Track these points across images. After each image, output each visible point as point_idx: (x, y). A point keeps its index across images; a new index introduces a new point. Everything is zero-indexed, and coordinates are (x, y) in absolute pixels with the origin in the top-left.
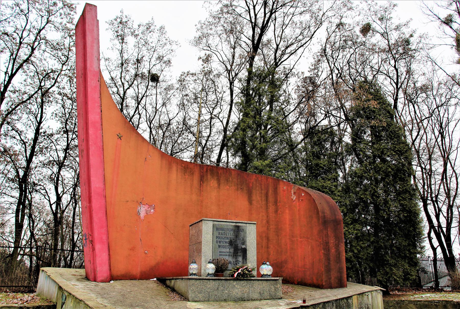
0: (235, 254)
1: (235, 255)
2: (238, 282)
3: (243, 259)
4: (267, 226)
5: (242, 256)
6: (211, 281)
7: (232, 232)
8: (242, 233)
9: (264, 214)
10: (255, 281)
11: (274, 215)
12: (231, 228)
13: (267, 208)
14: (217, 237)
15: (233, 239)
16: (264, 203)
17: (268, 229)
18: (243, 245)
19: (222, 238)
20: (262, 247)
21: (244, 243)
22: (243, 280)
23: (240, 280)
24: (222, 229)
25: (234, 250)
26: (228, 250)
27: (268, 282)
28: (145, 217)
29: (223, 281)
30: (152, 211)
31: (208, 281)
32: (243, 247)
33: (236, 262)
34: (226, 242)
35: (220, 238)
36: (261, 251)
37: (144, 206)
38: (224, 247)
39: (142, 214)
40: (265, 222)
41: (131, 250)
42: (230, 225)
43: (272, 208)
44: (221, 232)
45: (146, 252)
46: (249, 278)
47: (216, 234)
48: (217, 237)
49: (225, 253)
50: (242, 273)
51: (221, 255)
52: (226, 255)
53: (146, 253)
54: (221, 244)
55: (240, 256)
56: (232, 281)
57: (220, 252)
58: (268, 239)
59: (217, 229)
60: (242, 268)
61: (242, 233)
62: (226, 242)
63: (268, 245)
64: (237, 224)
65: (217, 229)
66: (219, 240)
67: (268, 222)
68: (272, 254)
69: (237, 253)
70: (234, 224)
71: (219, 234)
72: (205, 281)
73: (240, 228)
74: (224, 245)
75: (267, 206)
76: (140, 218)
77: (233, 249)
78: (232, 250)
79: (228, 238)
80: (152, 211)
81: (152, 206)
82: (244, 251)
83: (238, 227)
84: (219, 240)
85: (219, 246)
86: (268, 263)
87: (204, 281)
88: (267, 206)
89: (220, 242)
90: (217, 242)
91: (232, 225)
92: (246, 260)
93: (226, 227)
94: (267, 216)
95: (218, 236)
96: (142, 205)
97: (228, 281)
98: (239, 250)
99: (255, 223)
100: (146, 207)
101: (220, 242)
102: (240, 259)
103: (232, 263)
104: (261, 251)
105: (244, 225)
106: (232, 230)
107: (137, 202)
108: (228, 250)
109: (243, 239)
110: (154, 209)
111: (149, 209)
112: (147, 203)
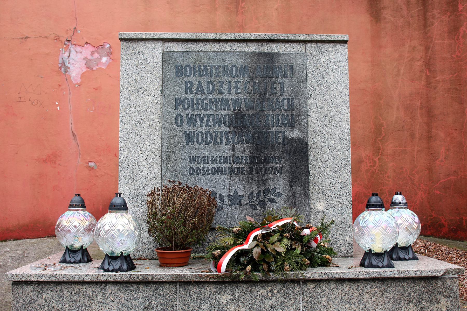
0: (257, 165)
1: (259, 171)
2: (238, 290)
3: (291, 183)
4: (428, 77)
5: (286, 170)
6: (111, 289)
7: (242, 80)
8: (287, 82)
9: (415, 43)
10: (324, 286)
11: (447, 42)
12: (240, 62)
13: (425, 26)
14: (179, 102)
15: (249, 108)
16: (414, 11)
17: (428, 84)
18: (292, 126)
19: (200, 105)
20: (412, 136)
21: (295, 117)
22: (264, 282)
23: (250, 282)
24: (200, 70)
25: (253, 150)
26: (226, 151)
27: (392, 287)
28: (83, 75)
29: (169, 291)
30: (104, 60)
31: (96, 289)
32: (294, 134)
33: (264, 198)
34: (217, 121)
35: (190, 103)
36: (408, 149)
37: (78, 49)
38: (210, 139)
39: (76, 69)
40: (418, 64)
41: (45, 161)
42: (234, 53)
43: (439, 25)
44: (195, 80)
45: (92, 164)
46: (292, 275)
47: (178, 89)
48: (179, 102)
49: (213, 161)
50: (256, 252)
51: (197, 171)
52: (220, 171)
53: (92, 169)
54: (198, 128)
55: (277, 171)
56: (210, 290)
57: (192, 160)
58: (429, 113)
59: (180, 71)
60: (263, 225)
61: (287, 82)
62: (217, 121)
63: (429, 132)
64: (267, 48)
65: (180, 71)
66: (190, 112)
67: (428, 64)
68: (441, 157)
69: (266, 161)
70: (253, 48)
71: (188, 90)
72: (84, 289)
73: (280, 61)
74: (212, 130)
75: (425, 19)
76: (68, 79)
77: (247, 147)
78: (244, 151)
79: (225, 103)
80: (104, 60)
81: (103, 46)
82: (298, 154)
83: (270, 56)
84: (190, 112)
85: (189, 138)
86: (399, 198)
87: (75, 288)
88: (425, 19)
89: (192, 120)
90: (178, 120)
91: (241, 54)
92: (305, 185)
93: (217, 62)
94: (427, 48)
95: (182, 96)
96: (72, 48)
97: (193, 289)
98: (274, 149)
99: (345, 38)
100: (87, 51)
101: (192, 120)
102: (280, 184)
103: (245, 200)
104: (408, 149)
105: (295, 48)
106: (241, 71)
107: (57, 38)
108: (226, 151)
109: (291, 106)
110: (109, 54)
111: (96, 55)
112: (86, 40)
